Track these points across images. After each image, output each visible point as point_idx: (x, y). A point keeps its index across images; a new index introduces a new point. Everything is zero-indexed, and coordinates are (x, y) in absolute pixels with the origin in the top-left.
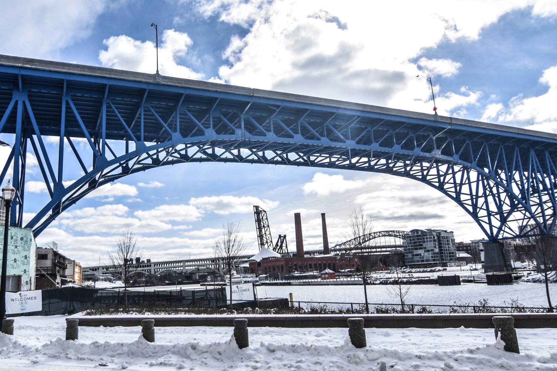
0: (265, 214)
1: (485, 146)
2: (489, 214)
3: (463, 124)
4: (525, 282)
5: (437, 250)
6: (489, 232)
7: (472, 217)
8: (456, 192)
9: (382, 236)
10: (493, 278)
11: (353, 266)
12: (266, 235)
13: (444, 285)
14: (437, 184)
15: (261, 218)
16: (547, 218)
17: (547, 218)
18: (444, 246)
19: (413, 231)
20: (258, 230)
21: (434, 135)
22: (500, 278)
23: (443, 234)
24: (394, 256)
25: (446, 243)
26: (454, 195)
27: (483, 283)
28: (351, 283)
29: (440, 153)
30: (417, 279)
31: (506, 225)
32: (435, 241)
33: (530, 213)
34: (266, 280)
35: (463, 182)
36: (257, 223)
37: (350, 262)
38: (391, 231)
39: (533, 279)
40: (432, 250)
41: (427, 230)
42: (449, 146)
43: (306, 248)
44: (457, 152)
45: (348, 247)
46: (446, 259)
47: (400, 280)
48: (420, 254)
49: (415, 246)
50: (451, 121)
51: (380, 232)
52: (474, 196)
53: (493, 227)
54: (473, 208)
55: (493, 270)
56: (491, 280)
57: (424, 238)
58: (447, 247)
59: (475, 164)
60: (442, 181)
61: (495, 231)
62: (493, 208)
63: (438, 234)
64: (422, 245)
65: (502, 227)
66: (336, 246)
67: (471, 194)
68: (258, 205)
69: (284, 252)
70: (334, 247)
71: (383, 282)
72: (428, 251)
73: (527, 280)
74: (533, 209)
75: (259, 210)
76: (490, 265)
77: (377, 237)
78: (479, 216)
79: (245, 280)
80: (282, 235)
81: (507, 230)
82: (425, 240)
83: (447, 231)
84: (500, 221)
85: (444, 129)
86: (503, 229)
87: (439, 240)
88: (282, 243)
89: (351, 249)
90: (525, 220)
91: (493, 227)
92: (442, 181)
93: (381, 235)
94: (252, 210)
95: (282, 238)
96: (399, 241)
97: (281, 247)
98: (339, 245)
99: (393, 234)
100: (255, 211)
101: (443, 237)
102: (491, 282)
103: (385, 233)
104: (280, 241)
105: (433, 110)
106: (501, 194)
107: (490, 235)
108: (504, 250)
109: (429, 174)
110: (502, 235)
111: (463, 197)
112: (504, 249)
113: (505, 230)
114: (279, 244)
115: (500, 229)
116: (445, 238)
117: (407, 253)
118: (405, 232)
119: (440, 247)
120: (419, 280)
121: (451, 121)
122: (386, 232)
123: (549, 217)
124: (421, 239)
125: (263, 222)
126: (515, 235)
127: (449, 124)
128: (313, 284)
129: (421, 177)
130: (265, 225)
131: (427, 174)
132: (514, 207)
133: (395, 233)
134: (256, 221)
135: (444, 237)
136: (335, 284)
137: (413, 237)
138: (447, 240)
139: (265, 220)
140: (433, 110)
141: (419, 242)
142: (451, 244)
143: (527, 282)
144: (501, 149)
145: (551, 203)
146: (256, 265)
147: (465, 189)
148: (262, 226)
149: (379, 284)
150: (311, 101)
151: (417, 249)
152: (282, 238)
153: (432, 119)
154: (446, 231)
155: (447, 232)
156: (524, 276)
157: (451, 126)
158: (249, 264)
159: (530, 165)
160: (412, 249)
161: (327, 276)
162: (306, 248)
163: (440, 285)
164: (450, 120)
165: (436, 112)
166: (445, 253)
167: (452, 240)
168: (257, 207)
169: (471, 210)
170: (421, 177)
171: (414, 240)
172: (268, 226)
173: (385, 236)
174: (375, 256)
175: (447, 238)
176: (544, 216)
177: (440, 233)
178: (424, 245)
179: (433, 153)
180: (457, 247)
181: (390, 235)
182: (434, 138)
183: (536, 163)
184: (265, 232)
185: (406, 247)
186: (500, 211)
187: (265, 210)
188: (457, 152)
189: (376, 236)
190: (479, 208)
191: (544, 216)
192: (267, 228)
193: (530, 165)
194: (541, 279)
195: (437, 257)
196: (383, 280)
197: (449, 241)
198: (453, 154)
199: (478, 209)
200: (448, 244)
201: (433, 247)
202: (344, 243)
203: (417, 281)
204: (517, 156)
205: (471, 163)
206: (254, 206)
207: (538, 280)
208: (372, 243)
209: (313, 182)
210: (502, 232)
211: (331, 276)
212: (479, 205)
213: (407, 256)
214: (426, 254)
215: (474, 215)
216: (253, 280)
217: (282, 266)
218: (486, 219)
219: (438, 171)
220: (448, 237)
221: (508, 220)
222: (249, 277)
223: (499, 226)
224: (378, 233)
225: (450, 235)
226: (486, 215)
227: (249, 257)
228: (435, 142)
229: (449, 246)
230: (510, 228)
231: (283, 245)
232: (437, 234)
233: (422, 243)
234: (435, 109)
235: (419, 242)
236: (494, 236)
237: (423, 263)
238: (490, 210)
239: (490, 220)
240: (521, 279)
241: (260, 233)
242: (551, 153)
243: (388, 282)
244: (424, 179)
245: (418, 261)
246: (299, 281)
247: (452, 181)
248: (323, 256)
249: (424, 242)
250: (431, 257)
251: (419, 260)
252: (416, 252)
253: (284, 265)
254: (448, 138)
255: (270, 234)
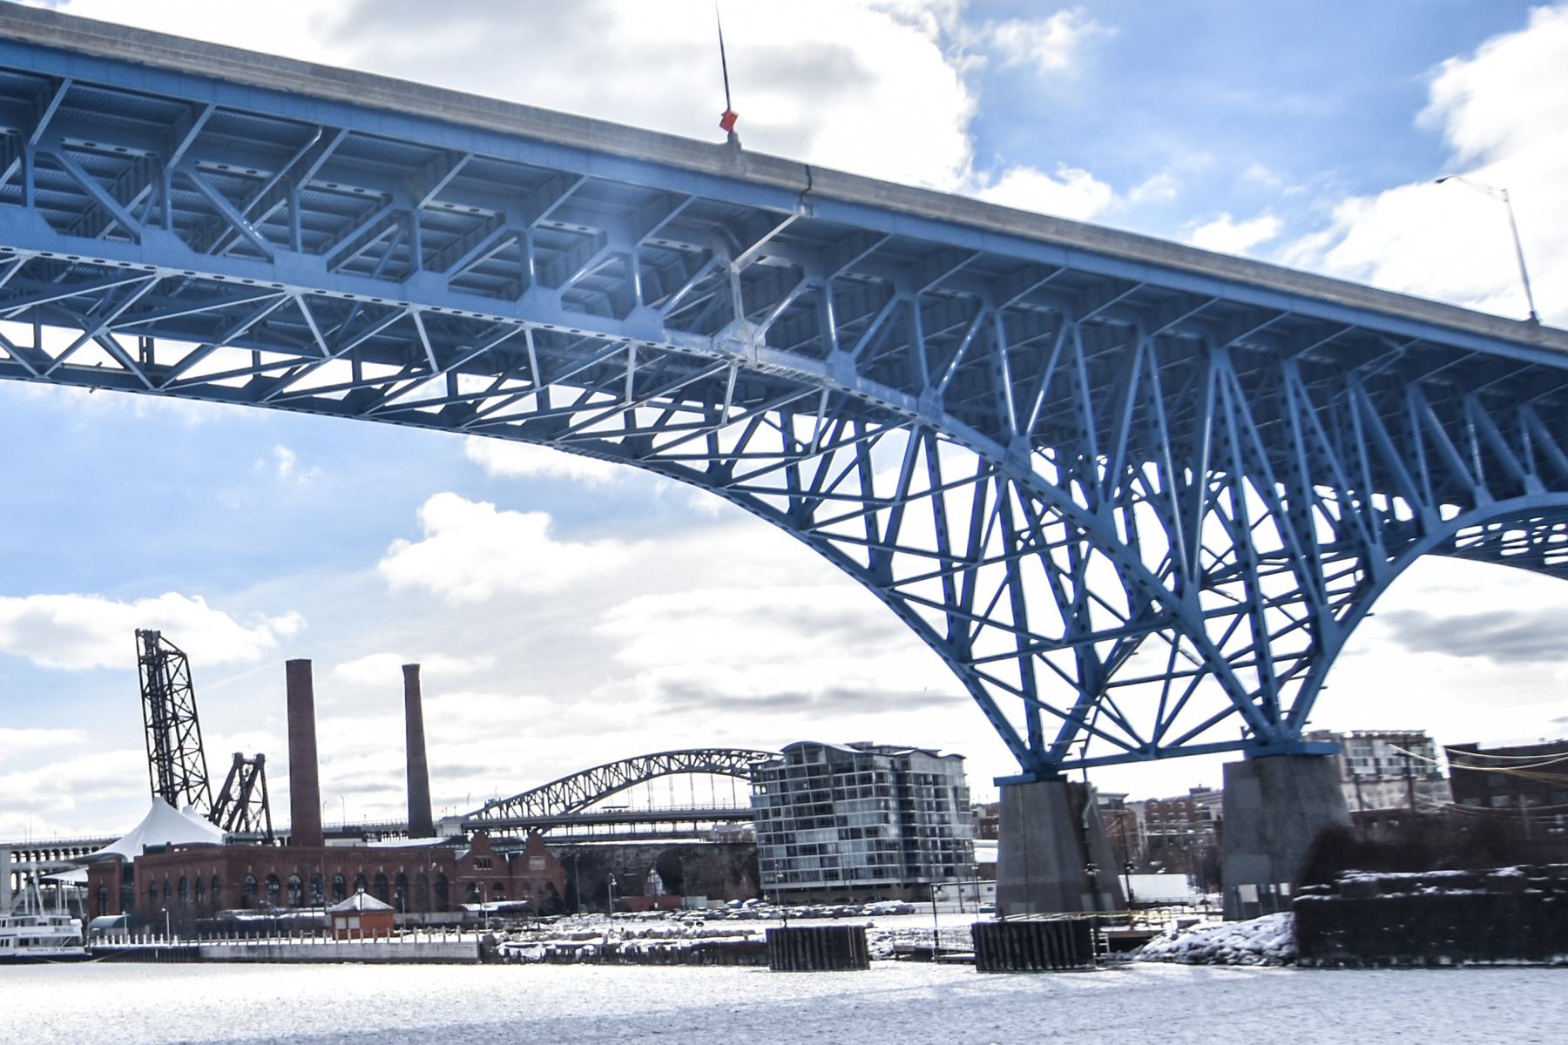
0: (194, 731)
1: (990, 321)
2: (1029, 648)
3: (870, 199)
4: (1157, 960)
5: (892, 832)
6: (1024, 735)
7: (946, 659)
8: (871, 540)
9: (679, 771)
10: (1002, 940)
11: (527, 886)
12: (182, 756)
13: (790, 970)
14: (782, 504)
15: (166, 682)
16: (1280, 668)
17: (1280, 668)
18: (923, 816)
19: (794, 751)
20: (151, 730)
21: (734, 256)
22: (1030, 939)
23: (918, 767)
24: (716, 851)
25: (929, 803)
26: (861, 555)
27: (962, 961)
28: (433, 954)
29: (761, 338)
30: (696, 941)
31: (1105, 703)
32: (883, 791)
33: (1200, 640)
34: (157, 939)
35: (823, 489)
36: (148, 702)
37: (511, 872)
38: (719, 752)
39: (1192, 947)
40: (873, 832)
41: (853, 746)
42: (808, 308)
43: (332, 816)
44: (846, 343)
45: (537, 811)
46: (928, 870)
47: (627, 944)
48: (823, 848)
49: (799, 811)
50: (810, 184)
51: (670, 755)
52: (958, 559)
53: (1042, 712)
54: (951, 620)
55: (1032, 905)
56: (992, 948)
57: (838, 782)
58: (935, 818)
59: (936, 400)
60: (806, 486)
61: (1052, 728)
62: (1046, 620)
63: (897, 765)
64: (828, 809)
65: (1087, 710)
66: (487, 808)
67: (944, 553)
68: (155, 629)
69: (253, 827)
70: (479, 813)
71: (559, 951)
72: (856, 834)
73: (1170, 951)
74: (1215, 629)
75: (158, 649)
76: (1019, 881)
77: (660, 774)
78: (976, 656)
79: (20, 936)
80: (249, 755)
81: (1104, 723)
82: (845, 787)
83: (940, 754)
84: (1080, 686)
85: (776, 219)
86: (1089, 722)
87: (903, 791)
88: (247, 787)
89: (549, 823)
90: (1174, 681)
91: (1042, 712)
92: (806, 486)
93: (674, 767)
94: (128, 652)
95: (245, 767)
96: (738, 793)
97: (243, 803)
98: (499, 804)
99: (727, 763)
100: (143, 652)
101: (917, 776)
102: (990, 956)
103: (693, 757)
104: (237, 780)
105: (721, 125)
106: (763, 423)
107: (1028, 746)
108: (1085, 816)
109: (746, 450)
110: (1083, 744)
111: (901, 567)
112: (1087, 809)
113: (1097, 726)
114: (235, 792)
115: (1075, 720)
116: (926, 783)
117: (768, 840)
118: (754, 755)
119: (905, 818)
120: (701, 946)
121: (810, 184)
122: (698, 753)
123: (1291, 663)
124: (826, 783)
125: (172, 700)
126: (1136, 745)
127: (802, 194)
128: (286, 955)
129: (702, 466)
130: (181, 713)
131: (739, 452)
132: (1140, 624)
133: (734, 760)
134: (144, 695)
135: (921, 779)
136: (368, 956)
137: (794, 772)
138: (937, 791)
139: (193, 757)
140: (721, 125)
141: (818, 797)
142: (952, 806)
143: (1165, 960)
144: (1070, 341)
145: (1302, 605)
146: (117, 876)
147: (917, 526)
148: (169, 715)
149: (543, 960)
150: (69, 35)
151: (808, 825)
152: (248, 770)
153: (712, 166)
154: (932, 754)
155: (935, 757)
156: (1162, 933)
157: (809, 207)
158: (88, 872)
159: (1209, 421)
160: (790, 825)
161: (354, 923)
162: (332, 816)
163: (773, 969)
164: (805, 178)
165: (732, 136)
166: (924, 844)
167: (955, 790)
168: (150, 638)
169: (941, 628)
170: (702, 466)
171: (799, 786)
172: (194, 718)
173: (690, 769)
174: (634, 851)
175: (935, 782)
176: (1263, 660)
177: (905, 761)
178: (841, 808)
179: (727, 335)
180: (983, 822)
181: (713, 769)
182: (736, 268)
183: (1237, 410)
184: (180, 741)
185: (765, 814)
186: (1079, 634)
187: (183, 649)
188: (846, 343)
189: (655, 772)
190: (977, 618)
191: (1263, 660)
192: (187, 725)
193: (1209, 421)
194: (1226, 950)
195: (891, 858)
196: (560, 942)
197: (946, 796)
198: (829, 350)
199: (974, 625)
200: (939, 807)
201: (875, 818)
202: (520, 799)
203: (694, 948)
204: (1146, 376)
205: (915, 392)
206: (138, 633)
207: (1212, 953)
208: (635, 799)
209: (429, 542)
210: (1082, 734)
211: (374, 924)
212: (979, 608)
213: (770, 852)
214: (847, 845)
215: (956, 651)
216: (57, 935)
217: (215, 878)
218: (1010, 671)
219: (790, 442)
220: (941, 780)
221: (1113, 680)
222: (40, 924)
223: (1072, 704)
224: (664, 758)
225: (948, 772)
226: (1014, 648)
227: (86, 846)
228: (736, 288)
229: (942, 816)
230: (1122, 722)
231: (251, 799)
232: (892, 762)
233: (830, 802)
234: (728, 120)
235: (818, 797)
236: (1048, 749)
237: (830, 884)
238: (1032, 629)
239: (1027, 673)
240: (1147, 948)
241: (159, 743)
242: (1309, 372)
243: (578, 952)
244: (718, 477)
245: (814, 876)
246: (235, 944)
247: (852, 486)
248: (404, 842)
249: (839, 795)
250: (865, 860)
251: (817, 872)
252: (803, 838)
253: (224, 879)
254: (806, 272)
255: (200, 750)
